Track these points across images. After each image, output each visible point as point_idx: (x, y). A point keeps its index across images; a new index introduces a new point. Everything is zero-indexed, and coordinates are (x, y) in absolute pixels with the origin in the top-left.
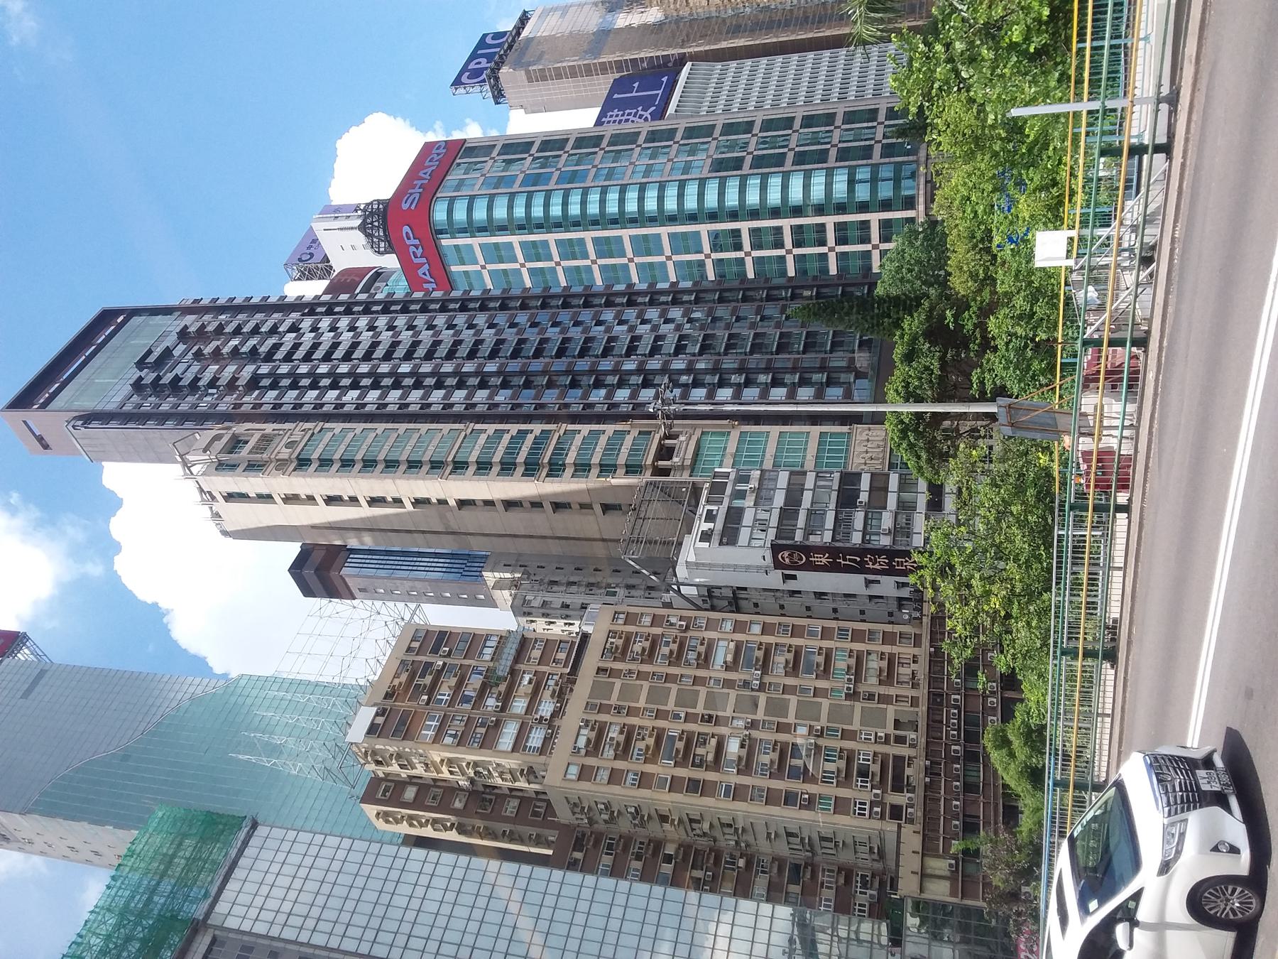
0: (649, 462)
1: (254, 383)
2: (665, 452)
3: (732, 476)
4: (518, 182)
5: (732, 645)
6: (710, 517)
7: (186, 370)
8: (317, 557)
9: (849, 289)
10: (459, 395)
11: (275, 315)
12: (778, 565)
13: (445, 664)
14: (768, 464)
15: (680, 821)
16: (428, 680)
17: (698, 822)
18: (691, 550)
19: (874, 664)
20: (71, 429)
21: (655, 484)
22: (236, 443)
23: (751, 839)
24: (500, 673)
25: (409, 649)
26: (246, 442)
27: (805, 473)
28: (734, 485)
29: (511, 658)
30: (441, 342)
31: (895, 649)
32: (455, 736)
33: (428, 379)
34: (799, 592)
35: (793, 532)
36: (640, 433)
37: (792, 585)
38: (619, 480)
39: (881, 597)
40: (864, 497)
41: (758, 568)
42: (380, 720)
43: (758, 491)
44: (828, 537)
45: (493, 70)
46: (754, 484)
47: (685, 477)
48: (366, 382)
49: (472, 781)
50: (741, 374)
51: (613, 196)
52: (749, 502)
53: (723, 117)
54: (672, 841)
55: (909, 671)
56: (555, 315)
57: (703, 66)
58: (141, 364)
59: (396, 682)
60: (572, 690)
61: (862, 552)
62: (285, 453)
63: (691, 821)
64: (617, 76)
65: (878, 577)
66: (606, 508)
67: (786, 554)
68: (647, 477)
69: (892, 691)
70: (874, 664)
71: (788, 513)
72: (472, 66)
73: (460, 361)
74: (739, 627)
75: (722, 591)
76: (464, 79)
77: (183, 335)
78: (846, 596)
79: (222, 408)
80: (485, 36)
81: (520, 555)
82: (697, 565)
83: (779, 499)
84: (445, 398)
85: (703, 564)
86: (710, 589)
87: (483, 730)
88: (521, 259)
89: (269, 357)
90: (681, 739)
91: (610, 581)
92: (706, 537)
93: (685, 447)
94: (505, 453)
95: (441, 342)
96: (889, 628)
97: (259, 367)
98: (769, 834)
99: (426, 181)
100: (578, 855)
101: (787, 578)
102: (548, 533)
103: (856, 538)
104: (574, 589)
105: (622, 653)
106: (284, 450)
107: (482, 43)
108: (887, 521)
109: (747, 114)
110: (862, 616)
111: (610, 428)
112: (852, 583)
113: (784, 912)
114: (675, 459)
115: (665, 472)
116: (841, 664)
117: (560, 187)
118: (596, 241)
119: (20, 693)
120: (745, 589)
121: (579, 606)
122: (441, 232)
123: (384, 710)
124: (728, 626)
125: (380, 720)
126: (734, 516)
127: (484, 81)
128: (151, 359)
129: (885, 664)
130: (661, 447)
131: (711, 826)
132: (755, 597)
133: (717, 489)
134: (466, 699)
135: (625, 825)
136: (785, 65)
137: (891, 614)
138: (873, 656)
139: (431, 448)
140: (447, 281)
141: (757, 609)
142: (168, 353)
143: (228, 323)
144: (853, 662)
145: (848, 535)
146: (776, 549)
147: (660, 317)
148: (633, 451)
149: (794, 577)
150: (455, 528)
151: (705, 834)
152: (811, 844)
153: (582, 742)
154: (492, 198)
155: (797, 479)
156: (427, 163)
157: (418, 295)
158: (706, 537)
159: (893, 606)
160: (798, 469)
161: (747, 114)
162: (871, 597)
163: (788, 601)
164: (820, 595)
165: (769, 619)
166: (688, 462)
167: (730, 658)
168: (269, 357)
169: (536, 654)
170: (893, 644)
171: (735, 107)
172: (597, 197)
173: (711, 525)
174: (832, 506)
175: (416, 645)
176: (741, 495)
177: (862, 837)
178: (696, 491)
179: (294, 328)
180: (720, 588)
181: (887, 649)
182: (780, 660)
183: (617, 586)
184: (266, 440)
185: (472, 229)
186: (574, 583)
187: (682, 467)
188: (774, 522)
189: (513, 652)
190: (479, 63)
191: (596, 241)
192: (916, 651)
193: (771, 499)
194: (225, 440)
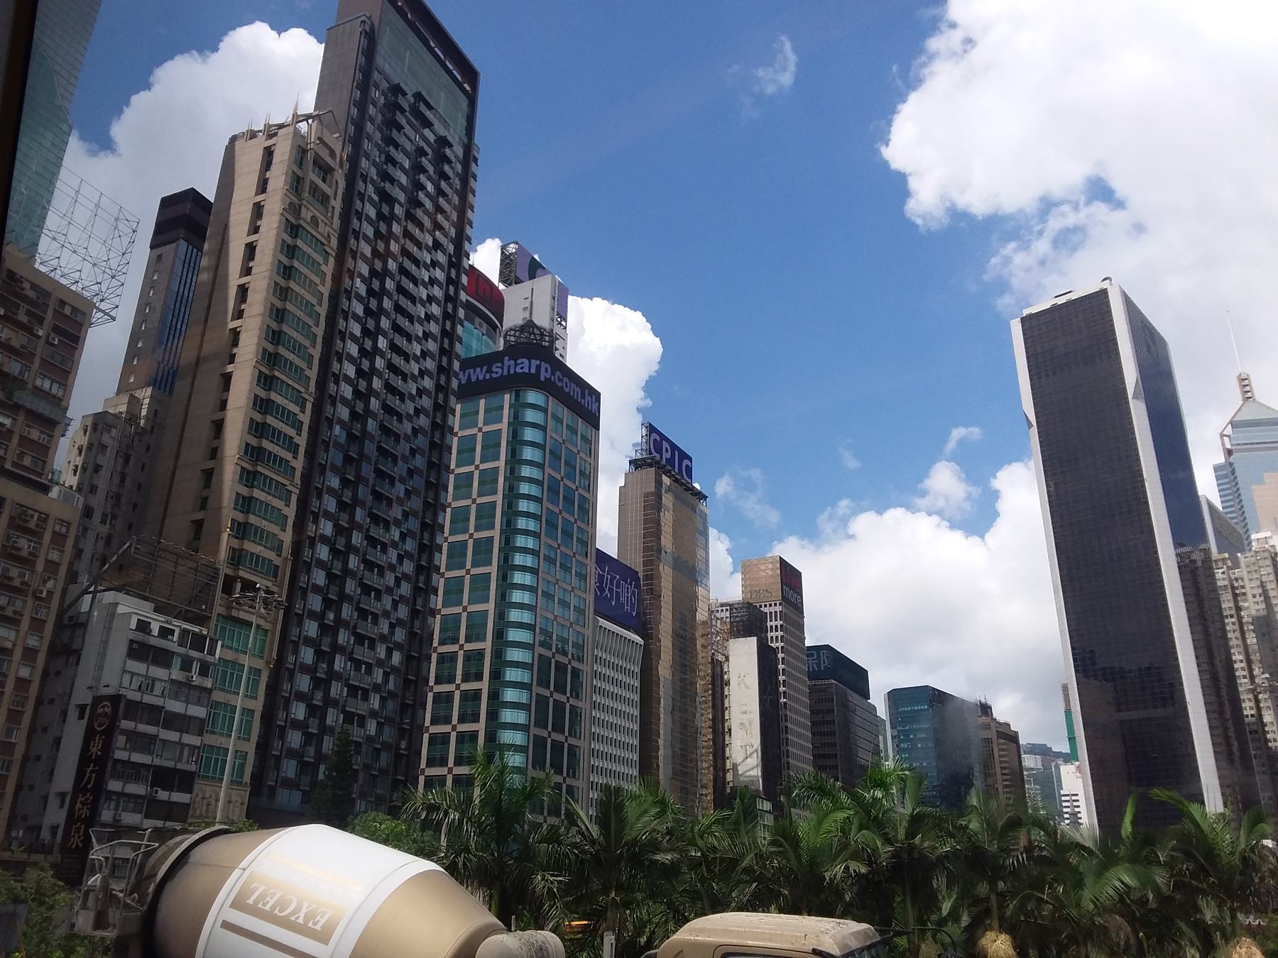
1: (386, 198)
3: (209, 659)
4: (554, 474)
6: (165, 633)
7: (409, 137)
13: (39, 337)
16: (23, 318)
18: (131, 609)
20: (363, 19)
21: (215, 577)
22: (325, 171)
24: (17, 394)
26: (324, 180)
27: (200, 734)
28: (200, 660)
29: (34, 408)
30: (414, 304)
33: (383, 246)
36: (277, 567)
37: (73, 714)
40: (163, 795)
41: (98, 679)
44: (120, 755)
45: (658, 462)
47: (218, 609)
51: (529, 561)
52: (176, 674)
56: (417, 493)
57: (639, 655)
58: (419, 97)
62: (307, 214)
64: (641, 575)
65: (66, 807)
66: (198, 525)
67: (108, 710)
71: (154, 714)
72: (665, 444)
76: (655, 436)
77: (443, 142)
78: (52, 773)
80: (690, 459)
83: (175, 706)
85: (111, 621)
86: (84, 626)
88: (484, 466)
89: (410, 216)
92: (143, 626)
94: (257, 528)
95: (414, 304)
104: (116, 480)
106: (310, 215)
107: (684, 456)
112: (65, 779)
117: (546, 477)
118: (490, 540)
120: (77, 664)
122: (517, 396)
124: (33, 642)
126: (162, 658)
127: (650, 453)
140: (470, 392)
142: (428, 124)
146: (116, 699)
149: (81, 717)
154: (541, 447)
157: (456, 365)
158: (143, 626)
169: (35, 434)
171: (595, 762)
175: (67, 311)
178: (201, 620)
179: (437, 246)
184: (324, 200)
185: (517, 424)
188: (148, 699)
189: (41, 410)
190: (667, 451)
191: (490, 540)
193: (176, 697)
194: (329, 160)
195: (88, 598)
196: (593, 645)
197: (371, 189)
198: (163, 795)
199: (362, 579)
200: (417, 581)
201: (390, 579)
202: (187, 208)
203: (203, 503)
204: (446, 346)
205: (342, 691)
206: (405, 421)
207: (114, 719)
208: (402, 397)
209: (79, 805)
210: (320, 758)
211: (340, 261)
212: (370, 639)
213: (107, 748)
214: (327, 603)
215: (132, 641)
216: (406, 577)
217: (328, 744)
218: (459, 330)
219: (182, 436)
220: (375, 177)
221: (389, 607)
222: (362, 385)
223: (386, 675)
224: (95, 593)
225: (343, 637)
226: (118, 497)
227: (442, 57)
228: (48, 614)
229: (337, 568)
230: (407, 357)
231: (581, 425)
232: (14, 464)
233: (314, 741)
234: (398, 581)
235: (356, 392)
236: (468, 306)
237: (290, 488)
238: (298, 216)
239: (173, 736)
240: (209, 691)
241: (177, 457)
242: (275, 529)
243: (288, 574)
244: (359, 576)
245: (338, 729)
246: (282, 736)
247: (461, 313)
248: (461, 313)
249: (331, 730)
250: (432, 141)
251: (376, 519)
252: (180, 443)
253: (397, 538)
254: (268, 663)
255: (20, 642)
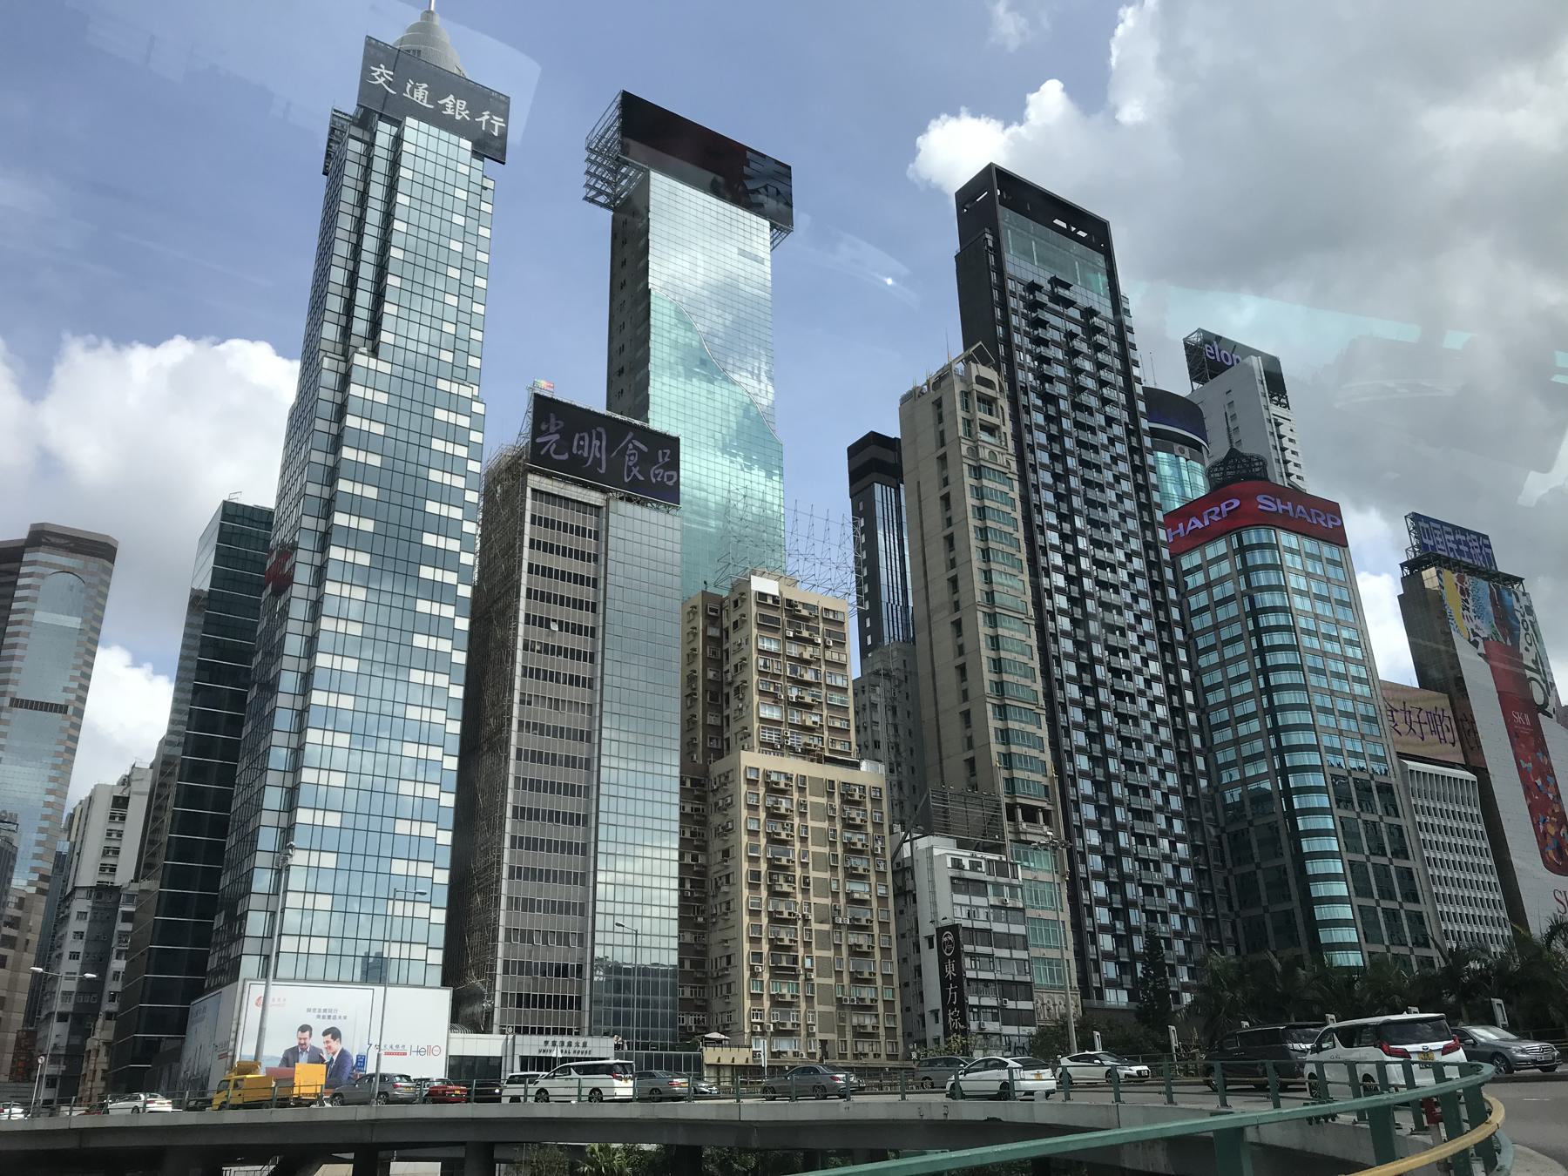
0: (1019, 800)
1: (1050, 399)
2: (1030, 814)
3: (1015, 882)
5: (867, 897)
6: (975, 866)
7: (1057, 325)
8: (889, 457)
9: (1214, 925)
10: (1071, 668)
11: (1122, 396)
12: (940, 931)
13: (818, 645)
14: (1030, 913)
15: (727, 867)
16: (805, 634)
17: (728, 882)
18: (942, 849)
19: (868, 1021)
21: (998, 809)
22: (989, 403)
23: (721, 924)
25: (827, 610)
26: (991, 414)
27: (1026, 949)
28: (1007, 885)
31: (882, 1039)
32: (765, 666)
33: (1058, 447)
34: (918, 951)
35: (971, 943)
36: (1046, 787)
37: (924, 944)
38: (996, 748)
39: (924, 1025)
40: (1011, 1005)
41: (935, 913)
42: (770, 601)
43: (1003, 907)
44: (970, 974)
46: (1010, 903)
47: (1009, 836)
48: (1067, 527)
49: (730, 684)
50: (1102, 752)
52: (993, 901)
53: (1410, 824)
54: (708, 860)
55: (866, 1051)
57: (1475, 795)
58: (1055, 282)
59: (800, 607)
60: (812, 761)
61: (962, 1003)
62: (984, 453)
63: (728, 876)
65: (941, 1021)
66: (971, 762)
67: (951, 938)
68: (1004, 800)
69: (849, 1037)
70: (868, 1021)
71: (987, 936)
73: (1077, 453)
74: (882, 899)
75: (911, 882)
77: (1089, 313)
78: (921, 994)
79: (1021, 375)
81: (916, 674)
82: (931, 857)
83: (999, 927)
84: (1044, 484)
85: (932, 863)
86: (911, 870)
87: (772, 690)
89: (1077, 406)
90: (788, 861)
91: (903, 766)
92: (957, 864)
93: (1041, 833)
94: (1020, 755)
96: (899, 1032)
97: (1065, 398)
98: (726, 941)
99: (1291, 514)
100: (688, 784)
101: (930, 939)
102: (940, 708)
103: (973, 1000)
104: (891, 731)
105: (848, 800)
106: (987, 451)
108: (992, 1026)
109: (1416, 851)
110: (906, 1010)
111: (1047, 756)
112: (933, 999)
113: (673, 959)
114: (1024, 825)
115: (1012, 817)
116: (867, 994)
119: (742, 246)
120: (915, 902)
121: (876, 738)
123: (777, 602)
124: (882, 891)
125: (770, 601)
126: (977, 887)
128: (1061, 291)
129: (870, 1030)
130: (1035, 809)
131: (726, 893)
132: (910, 911)
133: (1001, 869)
134: (794, 670)
135: (716, 819)
136: (1484, 869)
137: (910, 1035)
138: (874, 1020)
139: (1000, 547)
141: (900, 913)
142: (1069, 303)
143: (1106, 335)
144: (868, 1002)
145: (978, 993)
146: (954, 928)
147: (1169, 788)
148: (1023, 735)
149: (931, 946)
150: (934, 619)
151: (718, 888)
152: (722, 976)
153: (774, 778)
155: (1019, 941)
156: (1313, 511)
158: (957, 864)
159: (917, 1037)
160: (1031, 942)
161: (1416, 851)
162: (923, 1016)
163: (910, 941)
164: (918, 970)
165: (893, 927)
166: (1023, 837)
167: (856, 896)
168: (1077, 406)
170: (887, 1037)
172: (1287, 641)
173: (967, 867)
174: (999, 977)
176: (999, 893)
177: (735, 1017)
178: (998, 849)
179: (1110, 421)
180: (913, 878)
181: (882, 1031)
182: (861, 940)
183: (899, 773)
184: (991, 430)
186: (896, 730)
187: (1017, 832)
188: (977, 925)
192: (883, 1056)
193: (997, 920)
194: (989, 392)
195: (907, 846)
196: (1407, 794)
197: (1032, 396)
198: (1011, 1005)
199: (1129, 805)
200: (1185, 792)
201: (1150, 749)
202: (873, 451)
203: (970, 744)
204: (1143, 500)
205: (1133, 865)
206: (1110, 510)
207: (958, 944)
208: (1098, 469)
209: (950, 1019)
210: (1134, 957)
211: (1023, 479)
212: (1150, 837)
213: (959, 969)
214: (1100, 810)
215: (952, 878)
216: (1172, 791)
217: (1138, 944)
218: (1150, 460)
219: (934, 684)
220: (1030, 347)
221: (1156, 778)
222: (1072, 570)
223: (1184, 919)
224: (912, 840)
225: (1128, 865)
226: (897, 746)
227: (1064, 225)
228: (885, 867)
229: (1100, 774)
230: (1095, 449)
231: (1327, 551)
232: (831, 751)
233: (1125, 942)
234: (1158, 750)
235: (1068, 578)
236: (1153, 433)
237: (1037, 711)
238: (978, 459)
239: (1005, 953)
240: (1022, 910)
241: (936, 704)
242: (1034, 753)
243: (1057, 791)
244: (1119, 753)
245: (1144, 929)
246: (1094, 941)
247: (1147, 442)
248: (1147, 442)
249: (1137, 931)
250: (1079, 317)
251: (1097, 544)
252: (935, 690)
253: (1149, 731)
254: (1063, 876)
255: (873, 893)
